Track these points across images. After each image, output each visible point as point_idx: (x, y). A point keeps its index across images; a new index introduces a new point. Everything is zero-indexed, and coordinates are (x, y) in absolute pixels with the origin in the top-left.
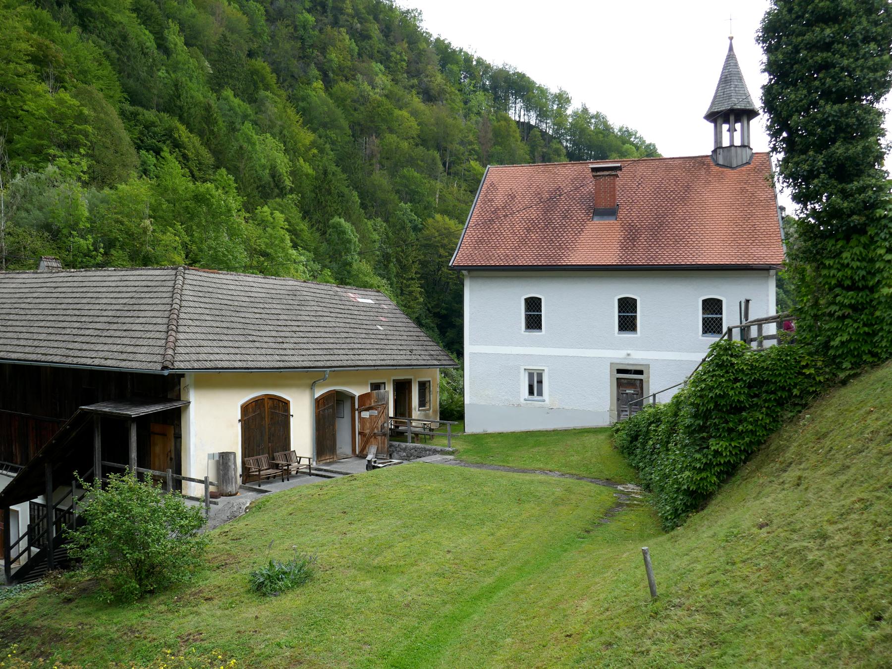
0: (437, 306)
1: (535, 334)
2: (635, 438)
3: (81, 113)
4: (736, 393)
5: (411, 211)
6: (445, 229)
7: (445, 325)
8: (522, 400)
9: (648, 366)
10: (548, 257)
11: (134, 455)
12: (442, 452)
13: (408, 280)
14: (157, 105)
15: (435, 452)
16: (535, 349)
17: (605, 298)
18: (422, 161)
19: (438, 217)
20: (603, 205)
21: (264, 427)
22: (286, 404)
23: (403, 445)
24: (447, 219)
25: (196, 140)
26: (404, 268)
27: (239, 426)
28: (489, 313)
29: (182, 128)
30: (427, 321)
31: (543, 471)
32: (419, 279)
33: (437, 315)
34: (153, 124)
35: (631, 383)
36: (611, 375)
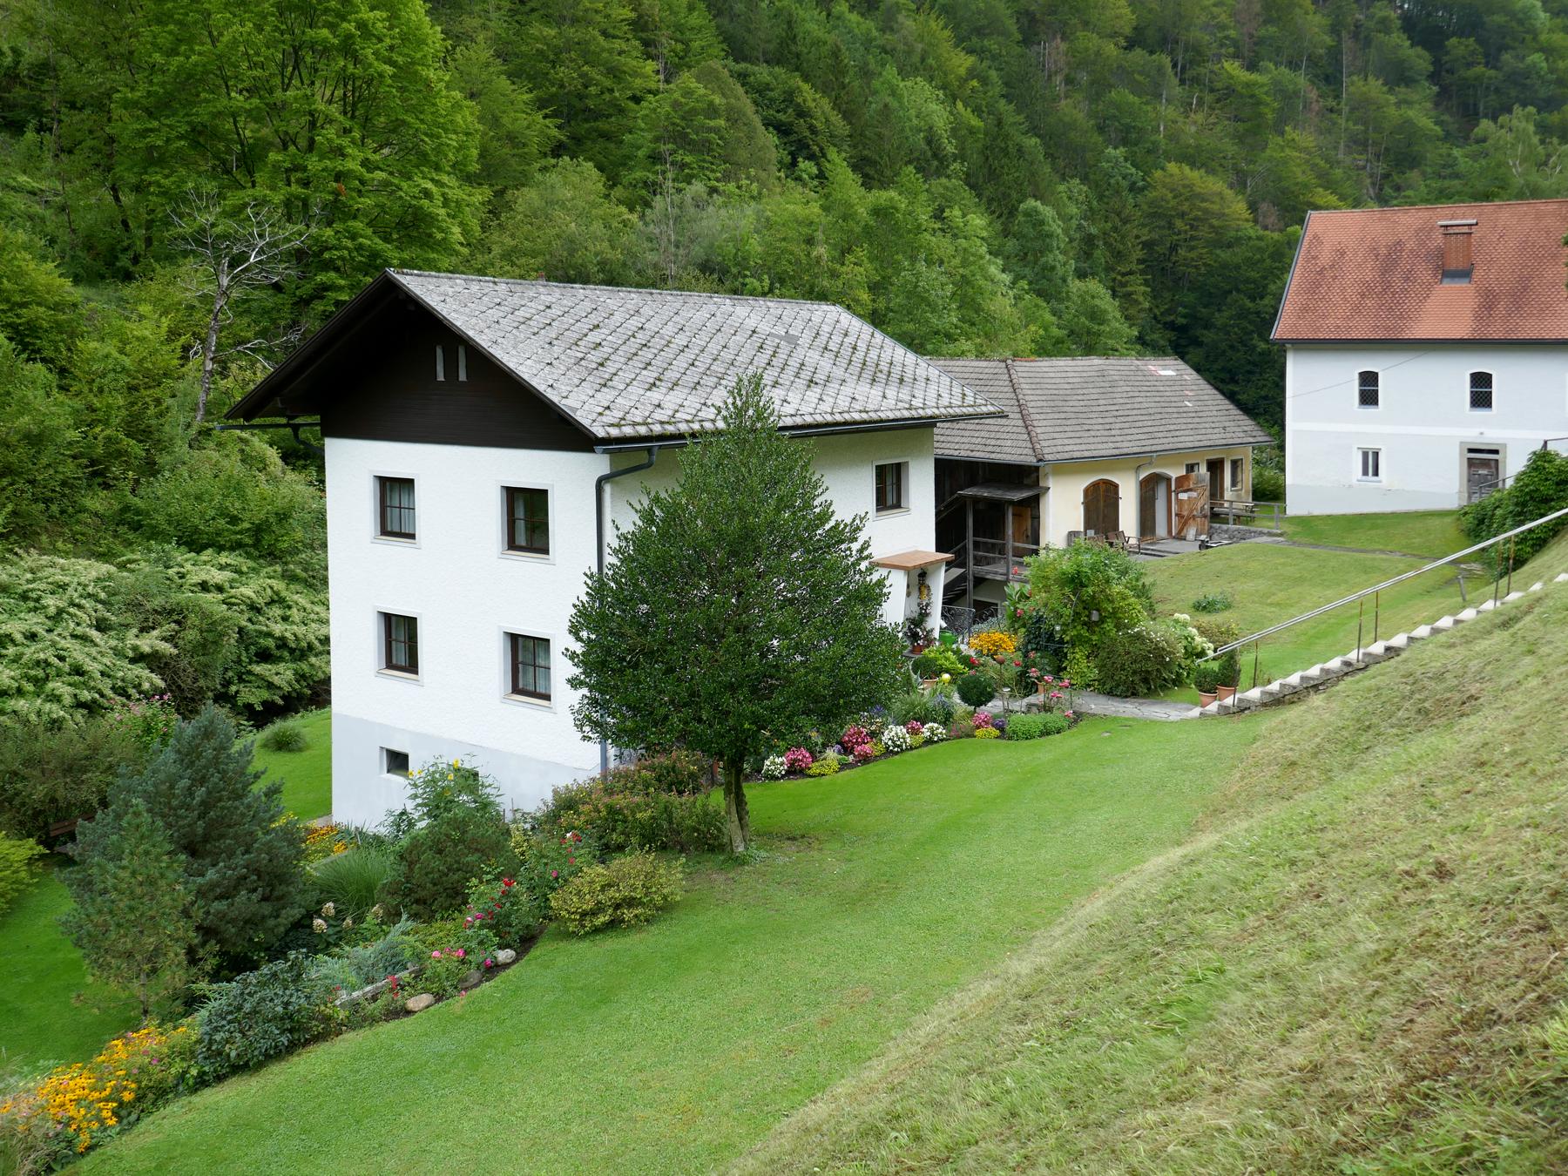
0: (1168, 312)
1: (1370, 410)
2: (1481, 521)
3: (711, 103)
4: (1547, 489)
5: (1126, 160)
6: (1184, 186)
7: (1267, 408)
8: (1354, 481)
9: (1505, 445)
10: (1387, 328)
11: (1010, 532)
12: (1270, 534)
13: (1124, 275)
14: (764, 53)
15: (1261, 534)
16: (1370, 427)
17: (1456, 372)
18: (1140, 73)
19: (1172, 167)
20: (1454, 263)
21: (1100, 505)
22: (1116, 486)
23: (1225, 527)
24: (1187, 169)
25: (825, 103)
26: (1119, 255)
27: (1082, 508)
28: (1315, 391)
29: (806, 87)
30: (1155, 336)
31: (1382, 551)
32: (1143, 272)
33: (1171, 326)
34: (768, 87)
35: (1485, 463)
36: (1461, 454)
